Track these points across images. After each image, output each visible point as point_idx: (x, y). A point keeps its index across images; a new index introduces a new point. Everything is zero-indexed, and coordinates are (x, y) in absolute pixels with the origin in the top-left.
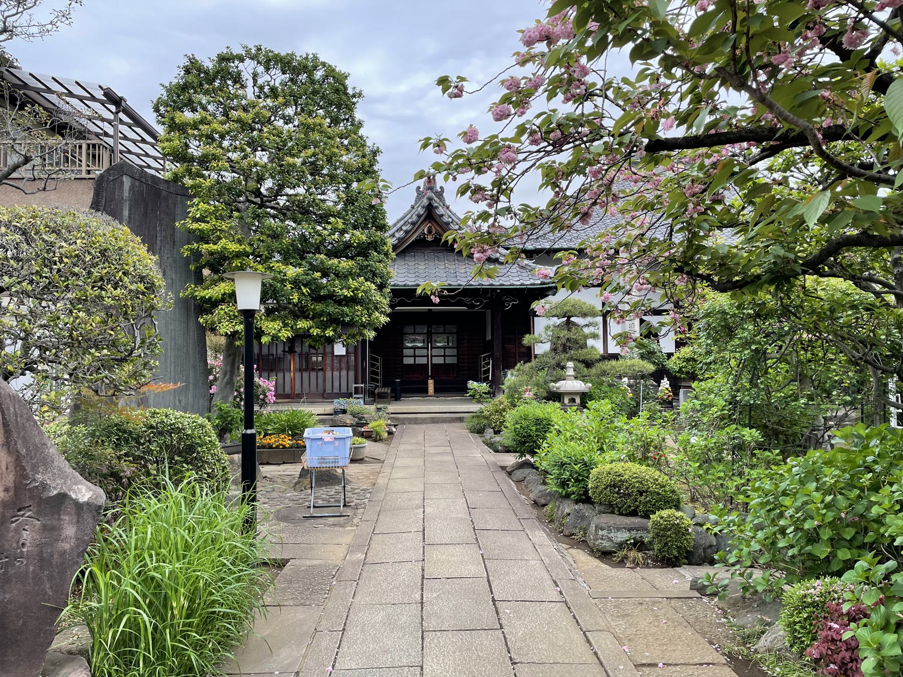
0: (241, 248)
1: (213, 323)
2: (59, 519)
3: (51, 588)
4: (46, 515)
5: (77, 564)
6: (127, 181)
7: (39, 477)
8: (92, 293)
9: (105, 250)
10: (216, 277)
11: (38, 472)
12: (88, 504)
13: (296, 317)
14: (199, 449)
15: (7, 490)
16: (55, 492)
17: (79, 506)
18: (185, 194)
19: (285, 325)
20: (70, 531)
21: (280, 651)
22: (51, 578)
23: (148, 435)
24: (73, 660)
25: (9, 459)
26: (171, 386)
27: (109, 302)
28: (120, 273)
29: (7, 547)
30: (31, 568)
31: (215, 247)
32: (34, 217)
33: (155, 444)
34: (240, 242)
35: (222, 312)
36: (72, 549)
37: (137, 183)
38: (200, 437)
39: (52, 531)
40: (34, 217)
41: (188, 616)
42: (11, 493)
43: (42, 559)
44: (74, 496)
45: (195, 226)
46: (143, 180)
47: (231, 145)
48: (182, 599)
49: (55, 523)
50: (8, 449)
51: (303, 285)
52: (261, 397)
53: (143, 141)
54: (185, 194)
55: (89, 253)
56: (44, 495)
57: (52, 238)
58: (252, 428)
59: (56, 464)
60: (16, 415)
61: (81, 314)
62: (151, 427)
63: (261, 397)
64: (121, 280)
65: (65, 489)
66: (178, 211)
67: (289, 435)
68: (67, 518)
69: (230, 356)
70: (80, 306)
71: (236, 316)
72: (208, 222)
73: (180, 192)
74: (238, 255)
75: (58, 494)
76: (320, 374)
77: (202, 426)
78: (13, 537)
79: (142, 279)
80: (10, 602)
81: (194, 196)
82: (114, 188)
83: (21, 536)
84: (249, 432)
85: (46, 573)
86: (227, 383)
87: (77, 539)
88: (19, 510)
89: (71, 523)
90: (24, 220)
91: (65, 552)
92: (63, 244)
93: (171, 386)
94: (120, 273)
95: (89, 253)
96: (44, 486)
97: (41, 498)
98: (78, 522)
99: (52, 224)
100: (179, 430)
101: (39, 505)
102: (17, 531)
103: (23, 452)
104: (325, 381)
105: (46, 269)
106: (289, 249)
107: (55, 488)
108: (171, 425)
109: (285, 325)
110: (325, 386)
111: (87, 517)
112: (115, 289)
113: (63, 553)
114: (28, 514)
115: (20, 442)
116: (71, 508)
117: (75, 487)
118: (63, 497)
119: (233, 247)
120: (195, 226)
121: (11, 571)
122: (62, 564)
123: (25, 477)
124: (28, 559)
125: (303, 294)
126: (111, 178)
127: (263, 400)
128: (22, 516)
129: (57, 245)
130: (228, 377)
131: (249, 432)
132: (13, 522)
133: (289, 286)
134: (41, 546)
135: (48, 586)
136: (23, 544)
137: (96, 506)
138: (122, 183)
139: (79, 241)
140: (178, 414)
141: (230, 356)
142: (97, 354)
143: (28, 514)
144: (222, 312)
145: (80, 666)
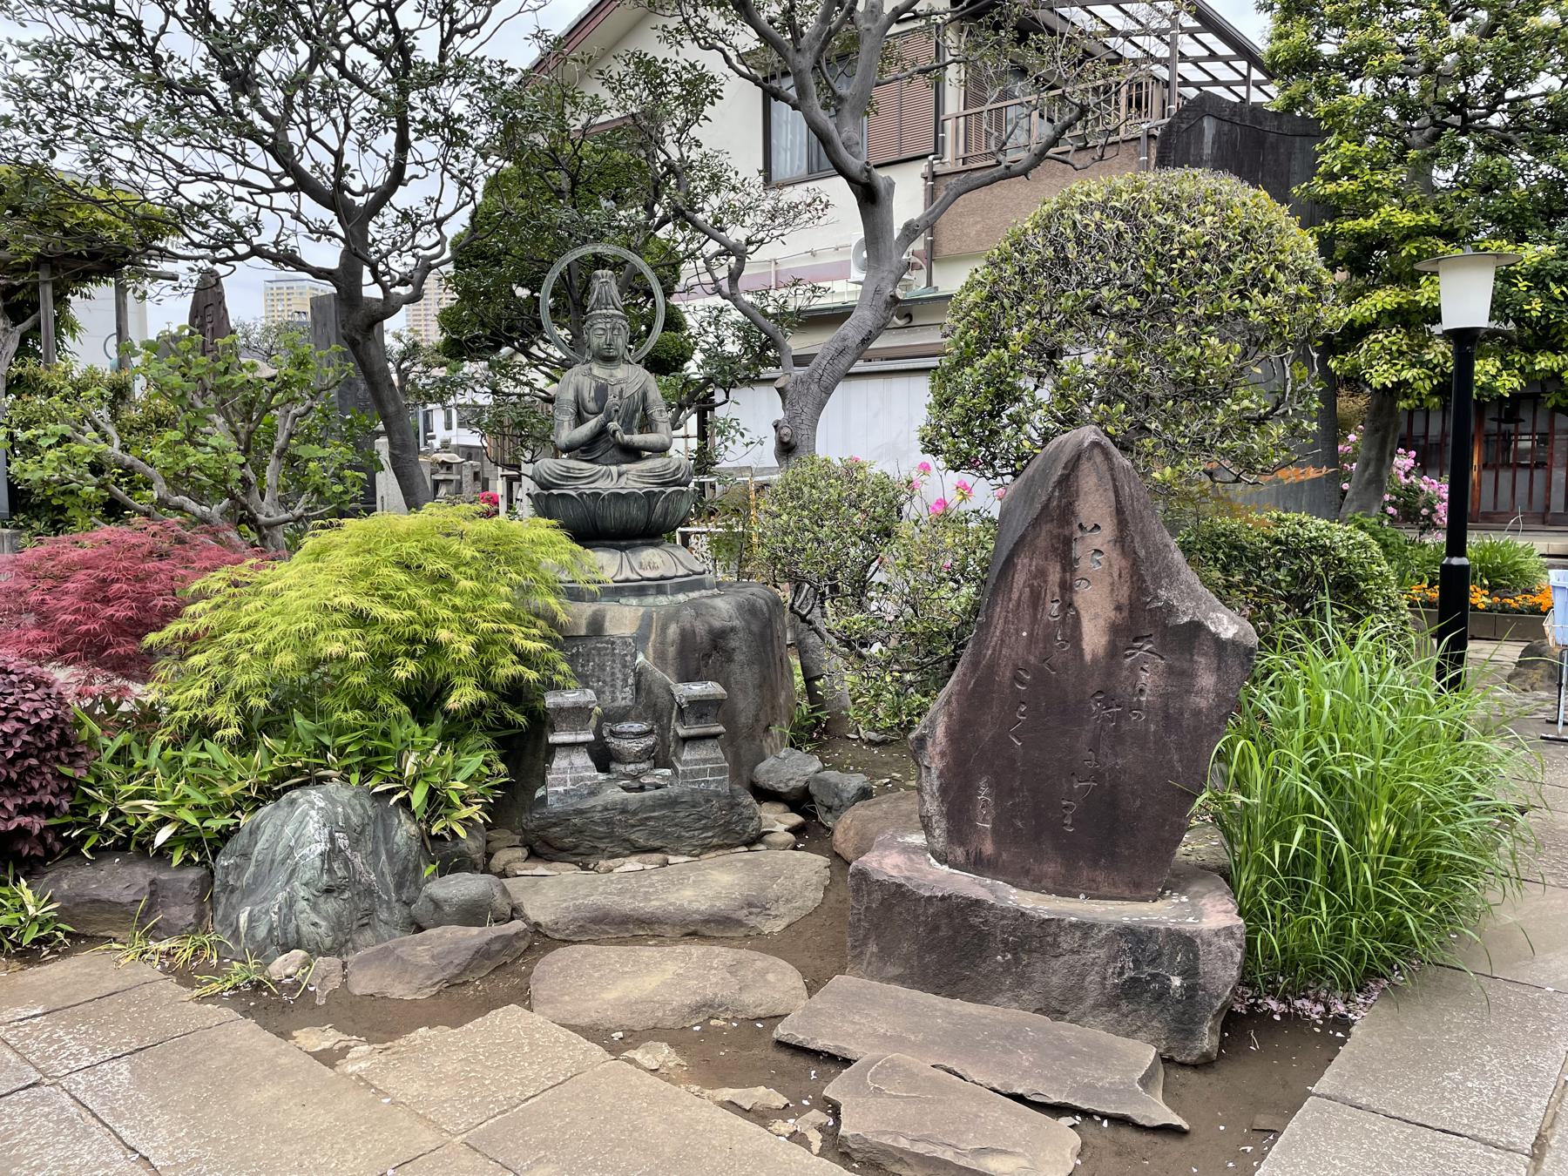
0: (1420, 220)
1: (1356, 368)
2: (1191, 660)
3: (1181, 761)
4: (1173, 651)
5: (1219, 733)
6: (1209, 125)
7: (1162, 593)
8: (1231, 303)
9: (1248, 231)
10: (1361, 282)
11: (1161, 587)
12: (1233, 642)
13: (1530, 350)
14: (1362, 585)
15: (1118, 608)
16: (1186, 619)
17: (1220, 645)
18: (1313, 131)
19: (1507, 365)
20: (1207, 680)
21: (1550, 956)
22: (1180, 747)
23: (1274, 556)
24: (1204, 877)
25: (1124, 563)
26: (1312, 473)
27: (1256, 318)
28: (1272, 268)
29: (1119, 690)
30: (1153, 727)
31: (1369, 223)
32: (1139, 190)
33: (1283, 571)
34: (1415, 207)
35: (1377, 347)
36: (1210, 709)
37: (1226, 127)
38: (1362, 566)
39: (1181, 676)
40: (1139, 190)
41: (1393, 852)
42: (1125, 614)
43: (1167, 717)
44: (1212, 628)
45: (1331, 187)
46: (1237, 120)
47: (487, 377)
48: (1383, 821)
49: (1186, 665)
50: (1123, 547)
51: (1554, 280)
52: (1425, 511)
53: (1213, 56)
54: (1313, 131)
55: (1224, 238)
56: (1171, 622)
57: (1169, 219)
58: (1462, 553)
59: (1183, 576)
60: (1131, 496)
61: (1214, 341)
62: (1277, 541)
63: (1425, 511)
64: (1273, 280)
65: (1199, 617)
66: (1296, 166)
67: (1483, 587)
68: (1202, 660)
69: (1377, 430)
70: (1211, 328)
71: (1401, 353)
72: (1355, 177)
73: (1300, 130)
74: (1411, 234)
75: (1191, 622)
76: (1539, 474)
77: (1364, 546)
78: (1127, 678)
79: (1303, 275)
80: (1124, 770)
81: (1329, 133)
82: (1188, 144)
83: (1138, 678)
84: (1455, 561)
85: (1173, 737)
86: (1369, 482)
87: (1218, 695)
88: (1136, 640)
89: (1208, 668)
90: (1125, 196)
91: (1200, 711)
92: (1187, 227)
93: (1312, 473)
94: (1272, 268)
95: (1224, 238)
96: (1170, 609)
97: (1166, 626)
98: (1219, 668)
99: (1166, 197)
100: (1324, 551)
101: (1163, 637)
102: (1132, 668)
103: (1142, 553)
104: (1548, 488)
105: (1161, 272)
106: (1523, 209)
107: (1184, 613)
108: (1310, 540)
109: (1507, 365)
110: (1548, 498)
111: (1233, 663)
112: (1265, 295)
113: (1197, 713)
114: (1148, 647)
115: (1137, 539)
116: (1208, 646)
117: (1212, 615)
118: (1196, 628)
119: (1406, 219)
120: (1331, 187)
121: (1125, 727)
122: (1196, 729)
123: (1143, 591)
124: (1148, 713)
125: (1555, 301)
126: (1184, 126)
127: (1428, 517)
128: (1140, 648)
129: (1177, 229)
130: (1371, 470)
131: (1455, 561)
132: (1127, 656)
133: (1523, 285)
134: (1165, 696)
135: (1176, 757)
136: (1141, 690)
137: (1246, 647)
138: (1202, 131)
139: (1208, 219)
140: (1321, 522)
141: (1377, 430)
142: (1235, 408)
143: (1148, 647)
144: (1377, 347)
145: (1218, 888)
